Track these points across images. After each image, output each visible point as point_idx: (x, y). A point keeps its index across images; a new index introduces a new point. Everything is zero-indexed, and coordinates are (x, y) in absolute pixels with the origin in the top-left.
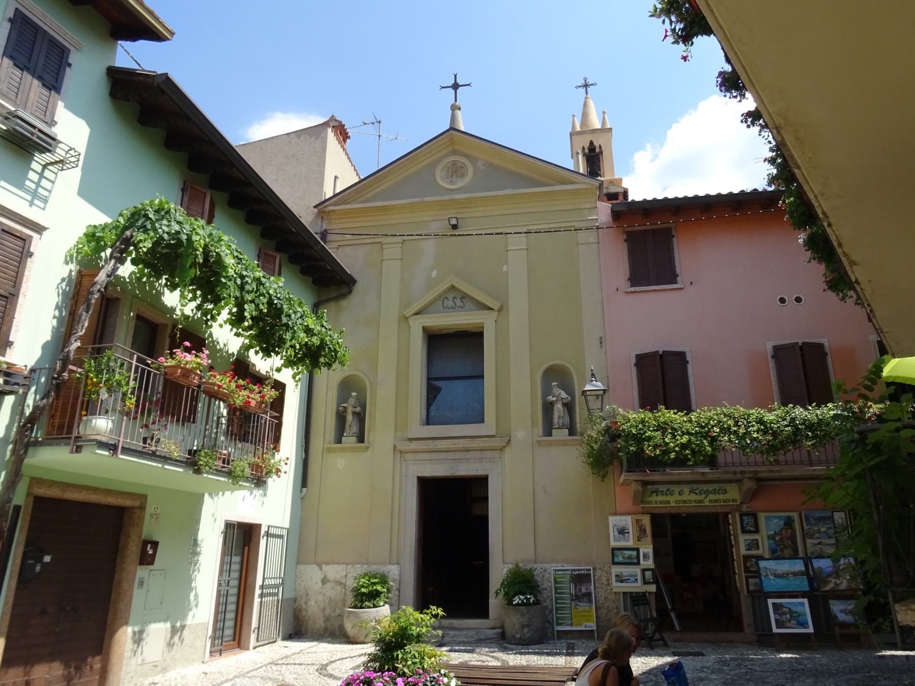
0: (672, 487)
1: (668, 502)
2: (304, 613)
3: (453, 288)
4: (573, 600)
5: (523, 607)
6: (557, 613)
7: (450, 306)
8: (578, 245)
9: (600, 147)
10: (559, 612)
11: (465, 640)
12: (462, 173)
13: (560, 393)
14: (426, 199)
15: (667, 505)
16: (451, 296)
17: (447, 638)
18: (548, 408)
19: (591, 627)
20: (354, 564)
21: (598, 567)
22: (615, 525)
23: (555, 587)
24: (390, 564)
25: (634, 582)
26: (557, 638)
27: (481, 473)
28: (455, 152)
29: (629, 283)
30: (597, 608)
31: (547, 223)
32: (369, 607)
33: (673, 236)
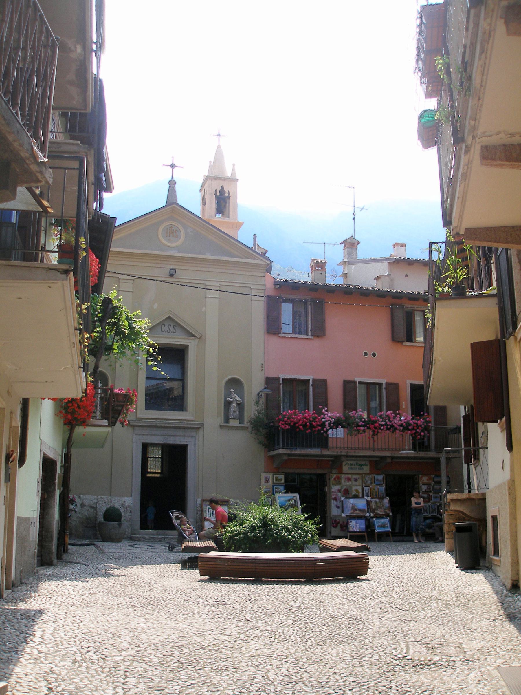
3: (169, 318)
7: (166, 331)
12: (177, 235)
18: (228, 404)
26: (421, 509)
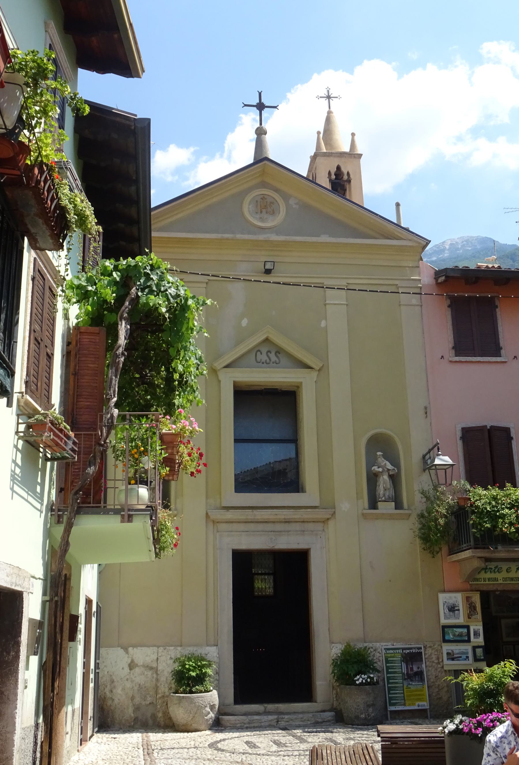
0: (500, 564)
1: (496, 579)
2: (109, 703)
4: (405, 679)
5: (367, 687)
6: (389, 693)
8: (400, 305)
9: (348, 174)
10: (391, 692)
11: (301, 723)
12: (273, 210)
13: (386, 464)
14: (239, 236)
15: (495, 582)
16: (264, 350)
17: (282, 722)
19: (424, 705)
20: (165, 646)
21: (428, 646)
22: (445, 602)
23: (386, 666)
24: (208, 646)
25: (465, 660)
26: (391, 717)
27: (302, 546)
28: (264, 185)
29: (454, 351)
30: (429, 687)
31: (368, 279)
32: (201, 692)
33: (497, 307)
